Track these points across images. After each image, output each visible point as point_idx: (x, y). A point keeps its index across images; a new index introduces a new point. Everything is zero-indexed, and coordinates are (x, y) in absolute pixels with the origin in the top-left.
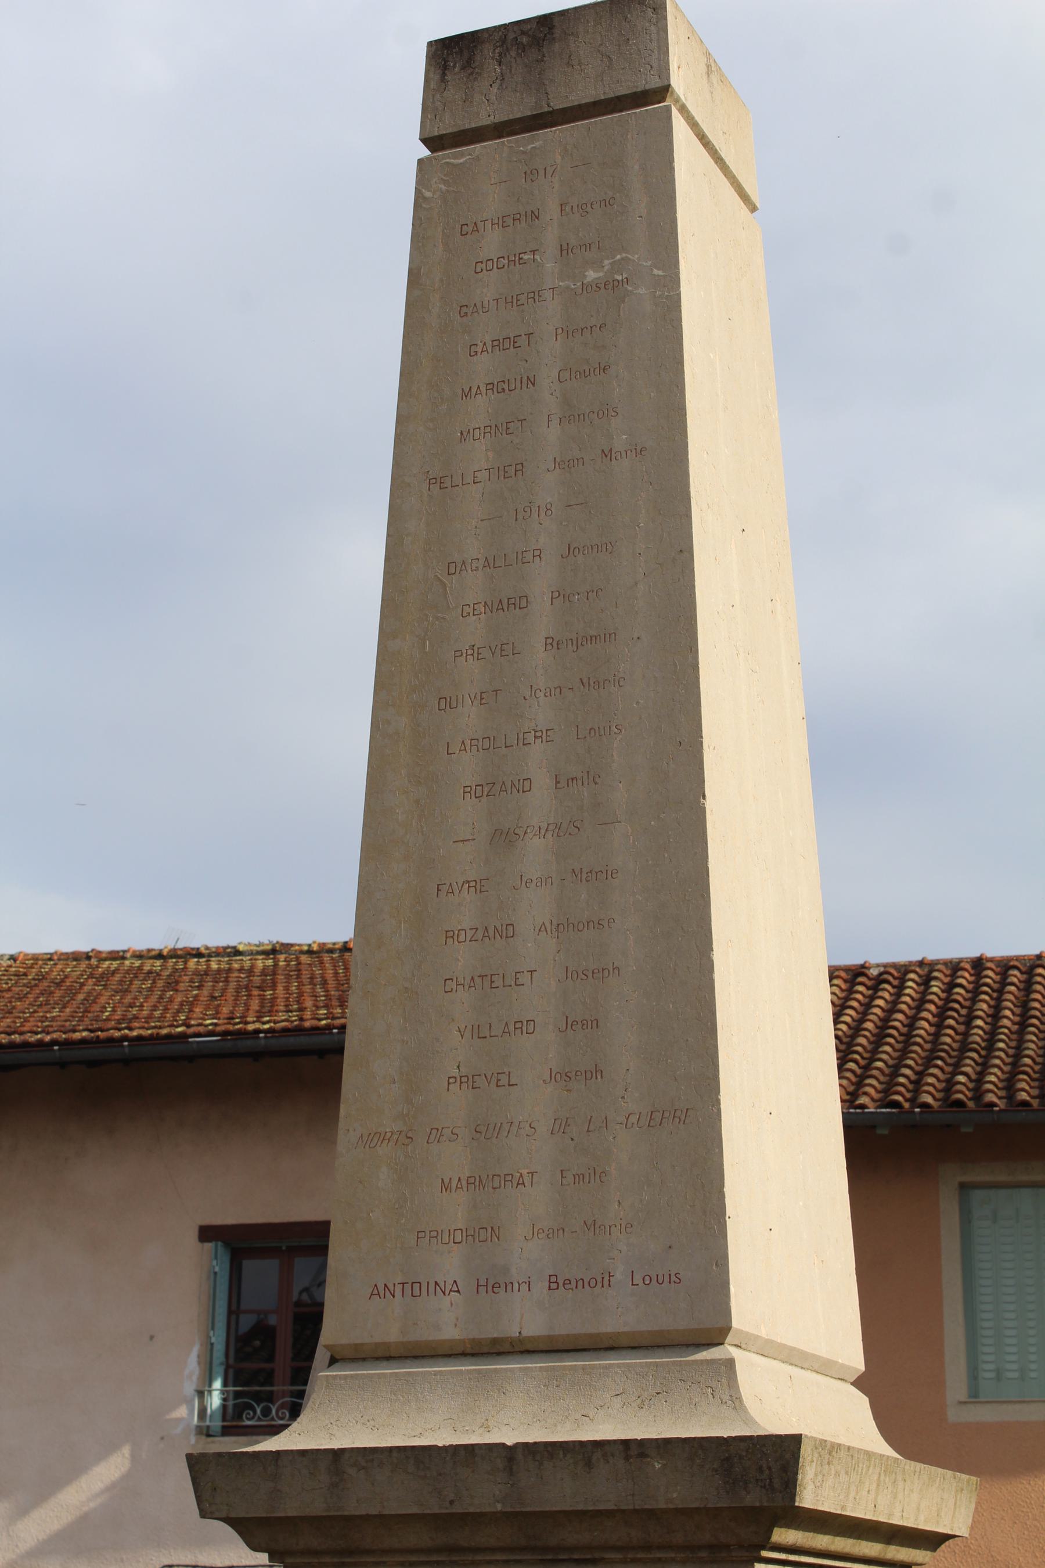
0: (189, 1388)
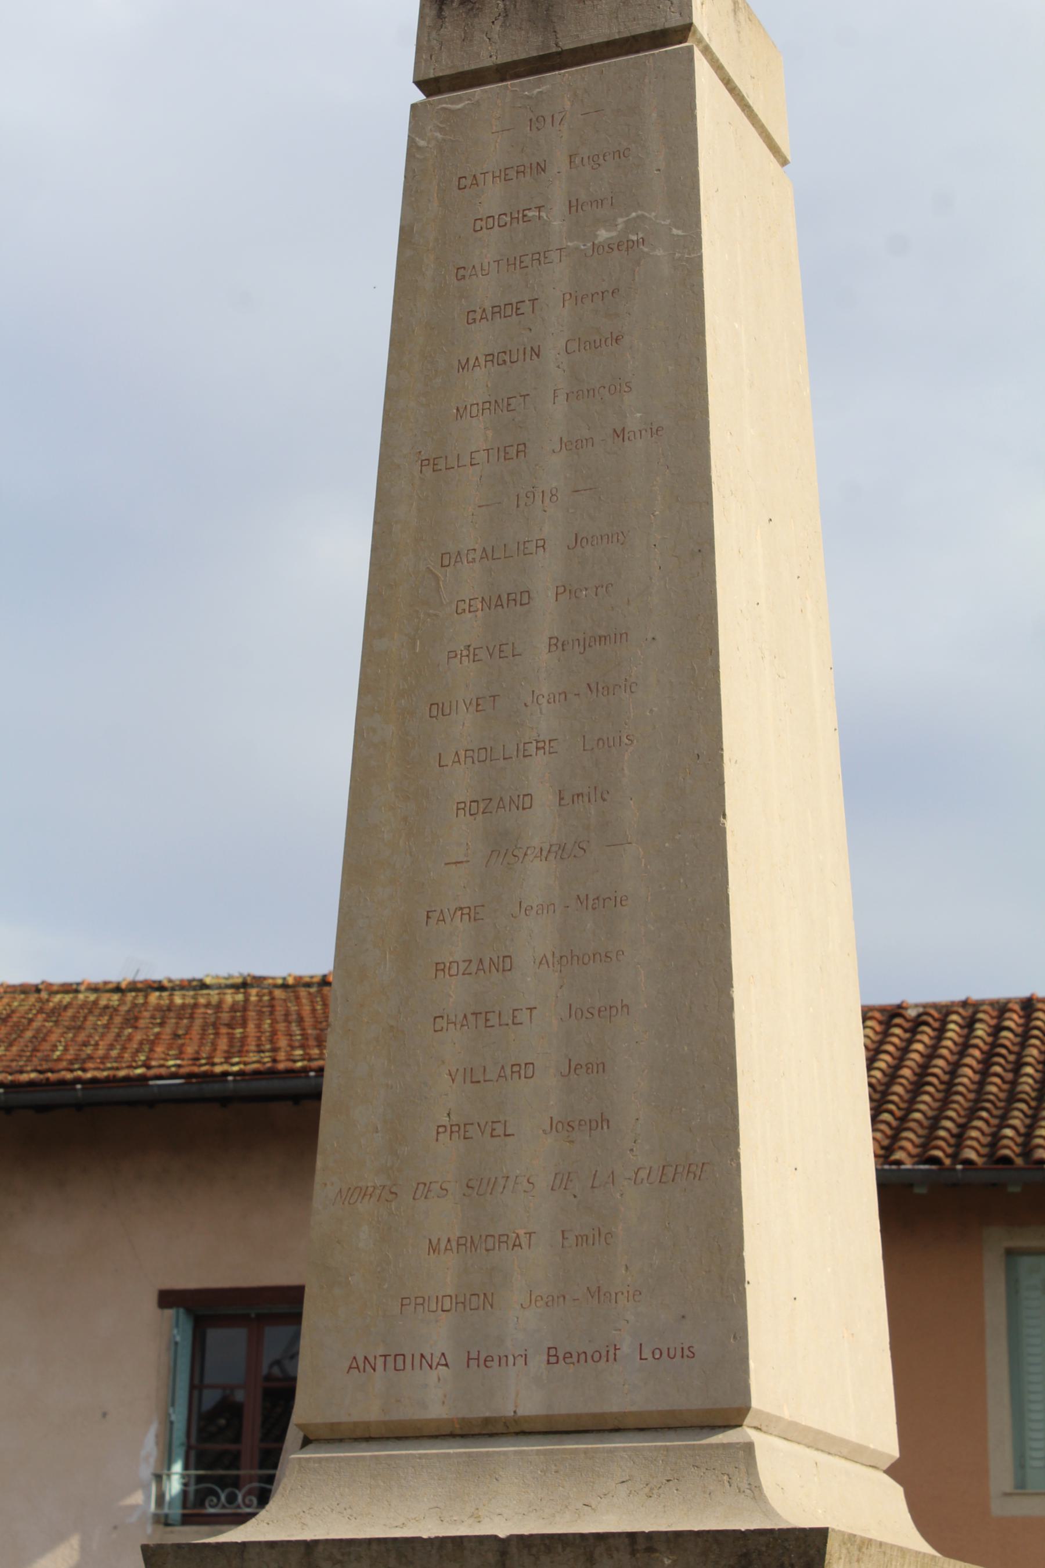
0: (146, 1471)
